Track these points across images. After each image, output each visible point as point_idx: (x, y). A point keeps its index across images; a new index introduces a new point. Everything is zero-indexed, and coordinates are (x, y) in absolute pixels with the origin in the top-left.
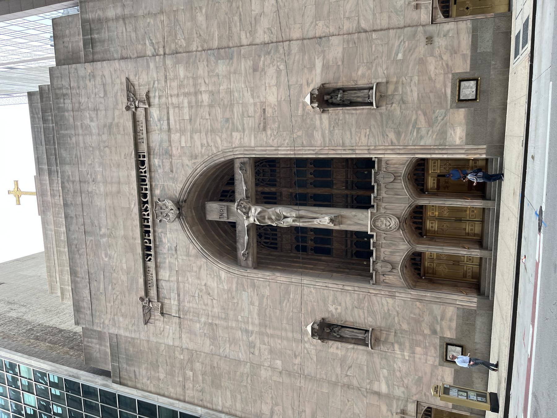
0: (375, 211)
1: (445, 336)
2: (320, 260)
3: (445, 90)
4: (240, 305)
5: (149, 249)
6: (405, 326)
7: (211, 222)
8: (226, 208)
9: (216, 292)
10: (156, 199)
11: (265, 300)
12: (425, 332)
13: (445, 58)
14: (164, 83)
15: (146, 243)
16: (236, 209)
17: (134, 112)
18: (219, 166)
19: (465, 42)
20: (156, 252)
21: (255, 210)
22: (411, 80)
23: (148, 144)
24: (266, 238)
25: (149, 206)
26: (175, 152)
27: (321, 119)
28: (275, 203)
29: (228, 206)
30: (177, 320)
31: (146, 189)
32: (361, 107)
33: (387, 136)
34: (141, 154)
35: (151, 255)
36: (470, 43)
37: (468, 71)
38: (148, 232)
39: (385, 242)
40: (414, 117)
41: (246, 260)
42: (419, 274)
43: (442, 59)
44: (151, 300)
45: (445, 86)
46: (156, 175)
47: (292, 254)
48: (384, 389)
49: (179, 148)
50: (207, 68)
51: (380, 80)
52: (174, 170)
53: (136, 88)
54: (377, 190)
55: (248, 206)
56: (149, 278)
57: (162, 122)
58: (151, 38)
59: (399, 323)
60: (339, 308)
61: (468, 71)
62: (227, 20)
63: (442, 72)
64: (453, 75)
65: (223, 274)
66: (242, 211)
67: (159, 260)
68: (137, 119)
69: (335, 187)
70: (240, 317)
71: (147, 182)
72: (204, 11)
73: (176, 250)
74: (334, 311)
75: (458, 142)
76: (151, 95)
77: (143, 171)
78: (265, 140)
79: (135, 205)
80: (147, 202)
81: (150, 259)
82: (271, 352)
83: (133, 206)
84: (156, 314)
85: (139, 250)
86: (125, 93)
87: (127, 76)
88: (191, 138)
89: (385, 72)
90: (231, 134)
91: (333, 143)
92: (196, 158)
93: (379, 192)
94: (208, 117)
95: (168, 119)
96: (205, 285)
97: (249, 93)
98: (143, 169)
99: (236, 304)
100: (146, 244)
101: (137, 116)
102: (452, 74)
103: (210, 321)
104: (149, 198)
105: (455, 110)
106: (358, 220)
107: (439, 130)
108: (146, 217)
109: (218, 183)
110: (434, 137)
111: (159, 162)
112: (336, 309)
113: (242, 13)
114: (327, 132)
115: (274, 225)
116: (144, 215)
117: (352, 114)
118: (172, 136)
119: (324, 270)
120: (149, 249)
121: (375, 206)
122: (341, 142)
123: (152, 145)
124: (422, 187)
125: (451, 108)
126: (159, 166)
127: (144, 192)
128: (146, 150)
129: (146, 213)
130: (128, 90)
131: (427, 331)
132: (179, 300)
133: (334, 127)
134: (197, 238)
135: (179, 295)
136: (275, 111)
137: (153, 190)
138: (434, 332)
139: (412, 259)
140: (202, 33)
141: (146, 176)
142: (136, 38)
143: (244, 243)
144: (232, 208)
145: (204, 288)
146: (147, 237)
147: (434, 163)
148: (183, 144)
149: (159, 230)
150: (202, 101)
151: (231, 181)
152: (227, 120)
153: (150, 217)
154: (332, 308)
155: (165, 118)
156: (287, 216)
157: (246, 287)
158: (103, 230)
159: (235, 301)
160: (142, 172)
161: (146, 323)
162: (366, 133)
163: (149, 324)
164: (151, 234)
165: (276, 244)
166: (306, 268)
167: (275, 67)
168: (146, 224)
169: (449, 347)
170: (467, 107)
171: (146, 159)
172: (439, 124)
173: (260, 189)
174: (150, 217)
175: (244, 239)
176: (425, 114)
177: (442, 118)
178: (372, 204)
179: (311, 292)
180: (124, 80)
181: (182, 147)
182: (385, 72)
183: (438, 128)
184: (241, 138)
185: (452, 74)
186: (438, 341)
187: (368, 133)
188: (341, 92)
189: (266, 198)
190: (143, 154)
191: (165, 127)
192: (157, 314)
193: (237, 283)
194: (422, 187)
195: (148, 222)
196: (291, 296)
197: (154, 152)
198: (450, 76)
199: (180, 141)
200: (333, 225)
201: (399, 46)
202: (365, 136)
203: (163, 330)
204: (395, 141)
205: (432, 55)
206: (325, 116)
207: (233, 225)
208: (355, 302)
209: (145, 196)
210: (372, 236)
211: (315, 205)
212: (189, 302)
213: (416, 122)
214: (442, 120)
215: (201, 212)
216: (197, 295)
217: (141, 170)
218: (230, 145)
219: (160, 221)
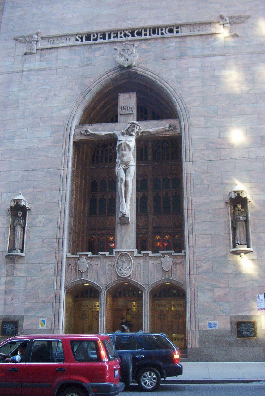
0: (136, 254)
2: (84, 205)
3: (245, 311)
4: (38, 129)
5: (88, 38)
7: (117, 98)
8: (131, 112)
9: (49, 105)
10: (136, 44)
11: (45, 154)
12: (26, 303)
15: (94, 36)
16: (130, 122)
18: (170, 104)
20: (85, 45)
21: (132, 142)
23: (189, 36)
24: (102, 152)
25: (130, 38)
26: (183, 62)
27: (218, 201)
28: (137, 160)
29: (133, 114)
31: (146, 35)
32: (231, 238)
33: (206, 263)
34: (179, 29)
35: (82, 41)
38: (104, 38)
40: (222, 285)
41: (81, 133)
42: (78, 296)
46: (159, 43)
47: (88, 177)
49: (187, 66)
52: (165, 61)
53: (242, 24)
54: (155, 256)
55: (134, 134)
56: (60, 40)
57: (210, 49)
59: (32, 280)
60: (42, 225)
66: (129, 128)
67: (77, 48)
69: (155, 217)
70: (26, 130)
71: (153, 36)
73: (87, 65)
74: (38, 220)
77: (163, 31)
78: (198, 149)
79: (130, 24)
80: (133, 36)
81: (77, 40)
83: (129, 22)
84: (25, 48)
85: (86, 30)
86: (237, 14)
88: (197, 78)
90: (203, 116)
91: (198, 213)
92: (178, 82)
93: (154, 258)
96: (55, 95)
98: (165, 31)
99: (38, 126)
100: (92, 36)
103: (20, 101)
104: (137, 37)
106: (127, 239)
108: (119, 35)
109: (155, 102)
110: (205, 304)
111: (172, 46)
115: (117, 160)
116: (121, 33)
118: (198, 59)
119: (75, 209)
120: (88, 38)
121: (139, 255)
123: (189, 40)
124: (158, 295)
125: (231, 317)
126: (169, 47)
127: (143, 32)
128: (184, 33)
129: (122, 35)
130: (239, 18)
131: (27, 305)
132: (39, 70)
133: (213, 213)
135: (44, 70)
137: (145, 41)
138: (27, 310)
139: (91, 290)
141: (158, 34)
143: (97, 131)
144: (132, 118)
145: (53, 93)
146: (99, 36)
147: (181, 305)
148: (191, 70)
149: (106, 48)
151: (156, 117)
153: (119, 39)
154: (41, 217)
156: (128, 173)
157: (55, 134)
159: (41, 125)
160: (162, 30)
161: (16, 39)
163: (15, 41)
164: (102, 40)
165: (97, 162)
166: (76, 191)
168: (112, 35)
170: (231, 330)
171: (175, 34)
173: (150, 144)
174: (119, 39)
175: (101, 130)
176: (225, 295)
177: (222, 309)
178: (142, 252)
179: (55, 198)
180: (248, 13)
181: (188, 68)
183: (213, 307)
184: (199, 125)
187: (207, 245)
188: (245, 219)
189: (145, 146)
190: (180, 31)
191: (207, 53)
192: (25, 50)
193: (59, 126)
194: (158, 295)
195: (114, 37)
196: (49, 179)
197: (182, 42)
199: (193, 67)
200: (120, 216)
202: (204, 243)
203: (9, 56)
204: (201, 270)
206: (222, 205)
207: (114, 119)
208: (48, 240)
209: (139, 34)
210: (111, 253)
211: (137, 199)
212: (38, 80)
213: (220, 287)
215: (126, 89)
216: (45, 87)
217: (164, 29)
219: (116, 49)
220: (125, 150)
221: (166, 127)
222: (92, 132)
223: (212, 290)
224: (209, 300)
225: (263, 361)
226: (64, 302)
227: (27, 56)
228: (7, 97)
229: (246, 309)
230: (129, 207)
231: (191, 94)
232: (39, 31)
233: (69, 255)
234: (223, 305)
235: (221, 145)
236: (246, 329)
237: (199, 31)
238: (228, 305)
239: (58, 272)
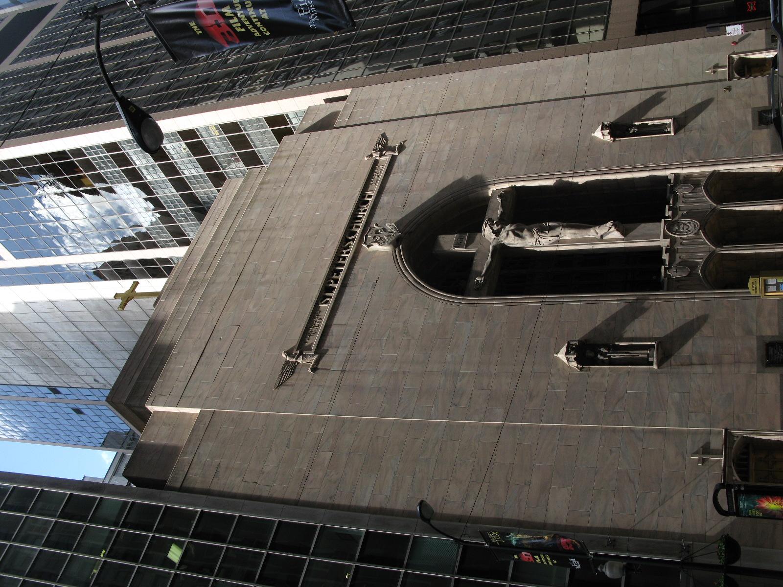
1: (764, 334)
30: (337, 375)
79: (333, 243)
195: (338, 275)
198: (750, 110)
214: (745, 138)
223: (720, 147)
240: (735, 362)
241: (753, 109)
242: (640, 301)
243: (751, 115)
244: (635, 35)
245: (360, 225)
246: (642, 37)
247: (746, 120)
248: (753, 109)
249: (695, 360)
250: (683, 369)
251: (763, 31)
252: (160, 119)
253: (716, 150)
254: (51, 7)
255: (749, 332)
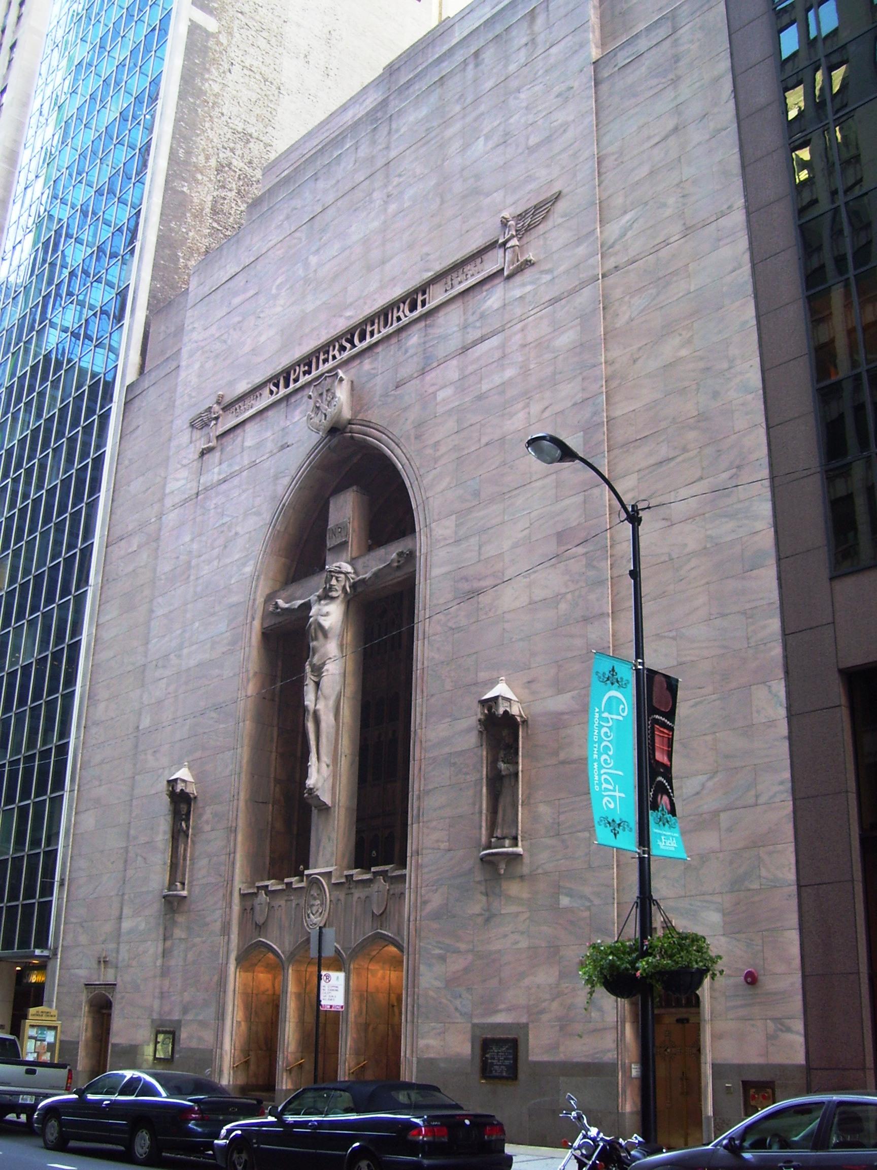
3: (501, 1011)
6: (190, 955)
11: (217, 672)
13: (555, 1005)
14: (548, 298)
15: (295, 371)
17: (497, 241)
19: (578, 1050)
22: (522, 933)
31: (372, 334)
36: (575, 1060)
37: (530, 1058)
39: (294, 905)
40: (463, 946)
43: (553, 1000)
44: (220, 420)
45: (508, 1010)
48: (126, 925)
50: (570, 404)
51: (526, 860)
58: (635, 225)
61: (530, 1058)
62: (663, 425)
63: (532, 1002)
64: (525, 1026)
65: (248, 569)
68: (485, 257)
72: (684, 352)
75: (422, 1043)
76: (528, 274)
82: (160, 702)
87: (564, 192)
89: (540, 871)
94: (484, 440)
95: (483, 339)
97: (521, 535)
101: (490, 253)
102: (527, 1024)
105: (468, 1036)
107: (440, 1003)
112: (207, 822)
113: (672, 464)
114: (447, 750)
117: (474, 804)
122: (430, 787)
126: (406, 351)
129: (336, 352)
130: (536, 208)
133: (455, 764)
134: (300, 488)
135: (225, 481)
136: (486, 614)
140: (639, 364)
142: (637, 183)
148: (441, 395)
150: (511, 415)
152: (477, 494)
155: (486, 330)
158: (313, 260)
162: (442, 842)
167: (563, 590)
169: (171, 1036)
170: (473, 1058)
172: (450, 1001)
176: (466, 970)
177: (459, 1007)
180: (555, 190)
182: (540, 871)
184: (445, 539)
185: (527, 1024)
186: (176, 1017)
198: (524, 1020)
201: (583, 897)
205: (562, 975)
213: (457, 951)
214: (456, 1009)
218: (436, 518)
220: (316, 639)
221: (392, 561)
222: (287, 606)
223: (443, 958)
224: (437, 984)
225: (59, 1057)
226: (237, 989)
227: (206, 457)
228: (178, 558)
229: (502, 1006)
230: (325, 771)
231: (436, 460)
232: (220, 393)
233: (243, 886)
234: (460, 996)
235: (479, 580)
236: (499, 1060)
237: (460, 283)
238: (470, 998)
239: (225, 929)
240: (162, 993)
241: (524, 1028)
242: (448, 542)
243: (510, 1021)
244: (841, 671)
245: (404, 319)
246: (837, 693)
247: (496, 1012)
248: (524, 1028)
249: (168, 943)
250: (161, 931)
251: (800, 1058)
252: (798, 27)
253: (437, 951)
254: (461, 1108)
255: (185, 1010)
